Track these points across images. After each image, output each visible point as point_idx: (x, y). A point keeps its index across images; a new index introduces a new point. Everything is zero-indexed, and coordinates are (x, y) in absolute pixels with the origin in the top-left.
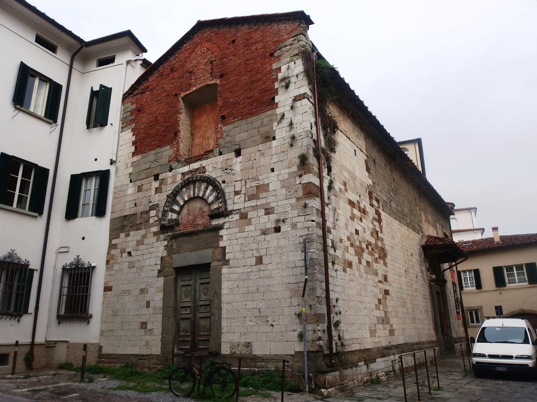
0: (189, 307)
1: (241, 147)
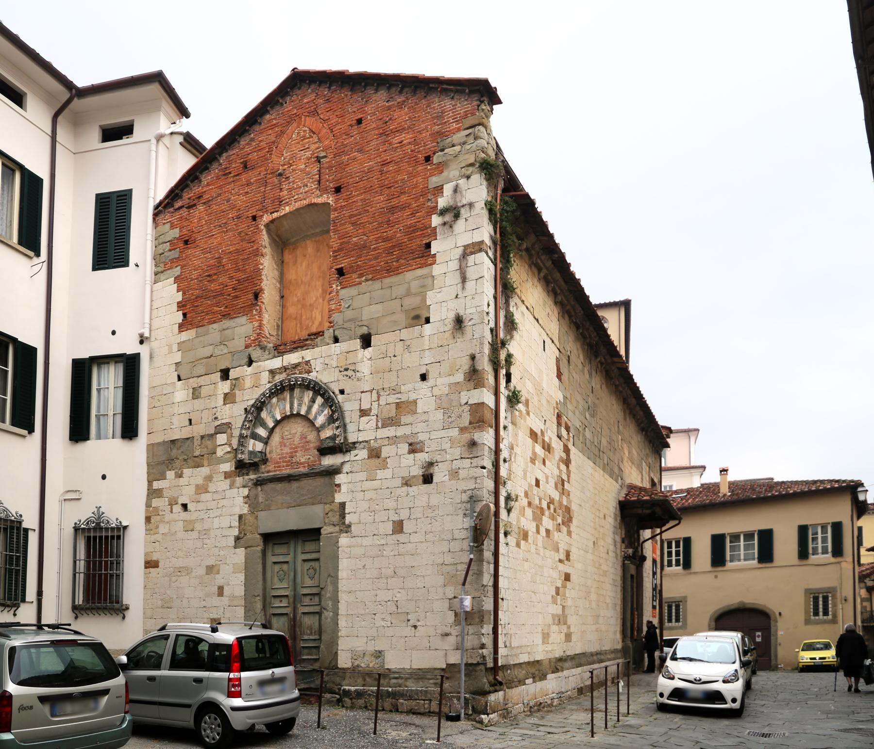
0: (287, 596)
1: (372, 332)
